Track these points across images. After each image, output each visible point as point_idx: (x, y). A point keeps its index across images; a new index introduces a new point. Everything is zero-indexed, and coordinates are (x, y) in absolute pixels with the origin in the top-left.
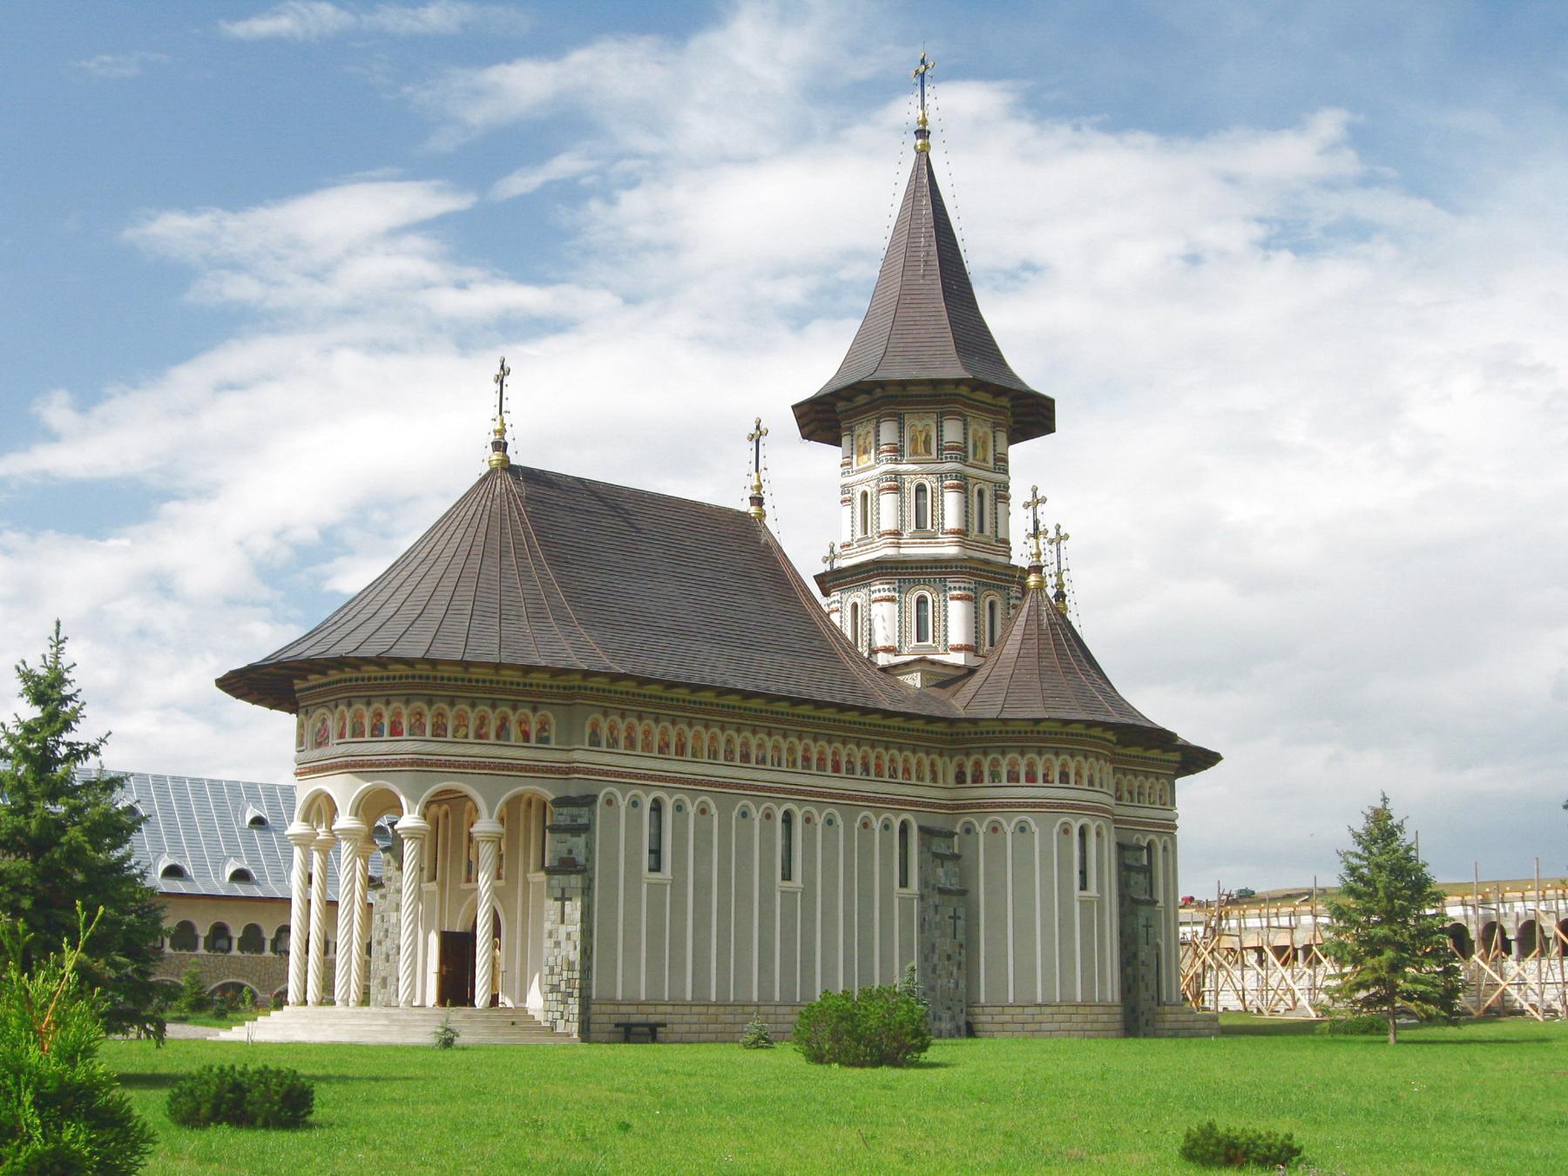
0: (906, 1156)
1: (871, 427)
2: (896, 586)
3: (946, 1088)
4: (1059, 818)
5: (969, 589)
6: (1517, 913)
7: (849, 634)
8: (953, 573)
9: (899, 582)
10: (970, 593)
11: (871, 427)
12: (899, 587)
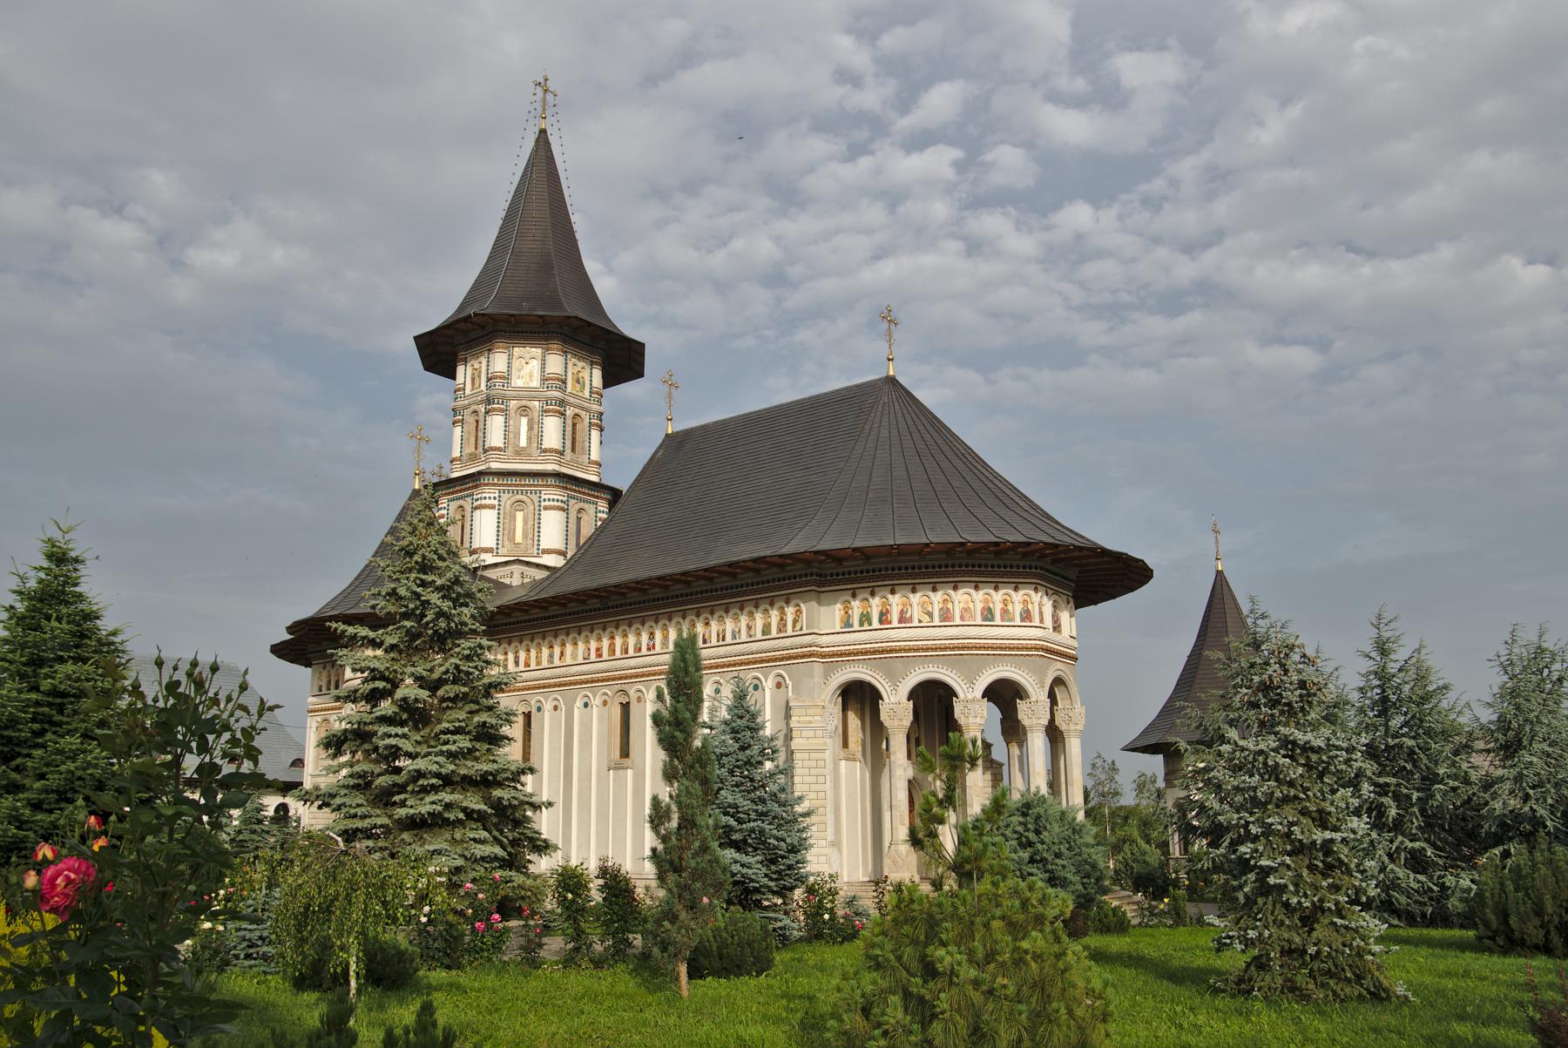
2: (497, 495)
10: (563, 505)
11: (537, 351)
12: (500, 496)
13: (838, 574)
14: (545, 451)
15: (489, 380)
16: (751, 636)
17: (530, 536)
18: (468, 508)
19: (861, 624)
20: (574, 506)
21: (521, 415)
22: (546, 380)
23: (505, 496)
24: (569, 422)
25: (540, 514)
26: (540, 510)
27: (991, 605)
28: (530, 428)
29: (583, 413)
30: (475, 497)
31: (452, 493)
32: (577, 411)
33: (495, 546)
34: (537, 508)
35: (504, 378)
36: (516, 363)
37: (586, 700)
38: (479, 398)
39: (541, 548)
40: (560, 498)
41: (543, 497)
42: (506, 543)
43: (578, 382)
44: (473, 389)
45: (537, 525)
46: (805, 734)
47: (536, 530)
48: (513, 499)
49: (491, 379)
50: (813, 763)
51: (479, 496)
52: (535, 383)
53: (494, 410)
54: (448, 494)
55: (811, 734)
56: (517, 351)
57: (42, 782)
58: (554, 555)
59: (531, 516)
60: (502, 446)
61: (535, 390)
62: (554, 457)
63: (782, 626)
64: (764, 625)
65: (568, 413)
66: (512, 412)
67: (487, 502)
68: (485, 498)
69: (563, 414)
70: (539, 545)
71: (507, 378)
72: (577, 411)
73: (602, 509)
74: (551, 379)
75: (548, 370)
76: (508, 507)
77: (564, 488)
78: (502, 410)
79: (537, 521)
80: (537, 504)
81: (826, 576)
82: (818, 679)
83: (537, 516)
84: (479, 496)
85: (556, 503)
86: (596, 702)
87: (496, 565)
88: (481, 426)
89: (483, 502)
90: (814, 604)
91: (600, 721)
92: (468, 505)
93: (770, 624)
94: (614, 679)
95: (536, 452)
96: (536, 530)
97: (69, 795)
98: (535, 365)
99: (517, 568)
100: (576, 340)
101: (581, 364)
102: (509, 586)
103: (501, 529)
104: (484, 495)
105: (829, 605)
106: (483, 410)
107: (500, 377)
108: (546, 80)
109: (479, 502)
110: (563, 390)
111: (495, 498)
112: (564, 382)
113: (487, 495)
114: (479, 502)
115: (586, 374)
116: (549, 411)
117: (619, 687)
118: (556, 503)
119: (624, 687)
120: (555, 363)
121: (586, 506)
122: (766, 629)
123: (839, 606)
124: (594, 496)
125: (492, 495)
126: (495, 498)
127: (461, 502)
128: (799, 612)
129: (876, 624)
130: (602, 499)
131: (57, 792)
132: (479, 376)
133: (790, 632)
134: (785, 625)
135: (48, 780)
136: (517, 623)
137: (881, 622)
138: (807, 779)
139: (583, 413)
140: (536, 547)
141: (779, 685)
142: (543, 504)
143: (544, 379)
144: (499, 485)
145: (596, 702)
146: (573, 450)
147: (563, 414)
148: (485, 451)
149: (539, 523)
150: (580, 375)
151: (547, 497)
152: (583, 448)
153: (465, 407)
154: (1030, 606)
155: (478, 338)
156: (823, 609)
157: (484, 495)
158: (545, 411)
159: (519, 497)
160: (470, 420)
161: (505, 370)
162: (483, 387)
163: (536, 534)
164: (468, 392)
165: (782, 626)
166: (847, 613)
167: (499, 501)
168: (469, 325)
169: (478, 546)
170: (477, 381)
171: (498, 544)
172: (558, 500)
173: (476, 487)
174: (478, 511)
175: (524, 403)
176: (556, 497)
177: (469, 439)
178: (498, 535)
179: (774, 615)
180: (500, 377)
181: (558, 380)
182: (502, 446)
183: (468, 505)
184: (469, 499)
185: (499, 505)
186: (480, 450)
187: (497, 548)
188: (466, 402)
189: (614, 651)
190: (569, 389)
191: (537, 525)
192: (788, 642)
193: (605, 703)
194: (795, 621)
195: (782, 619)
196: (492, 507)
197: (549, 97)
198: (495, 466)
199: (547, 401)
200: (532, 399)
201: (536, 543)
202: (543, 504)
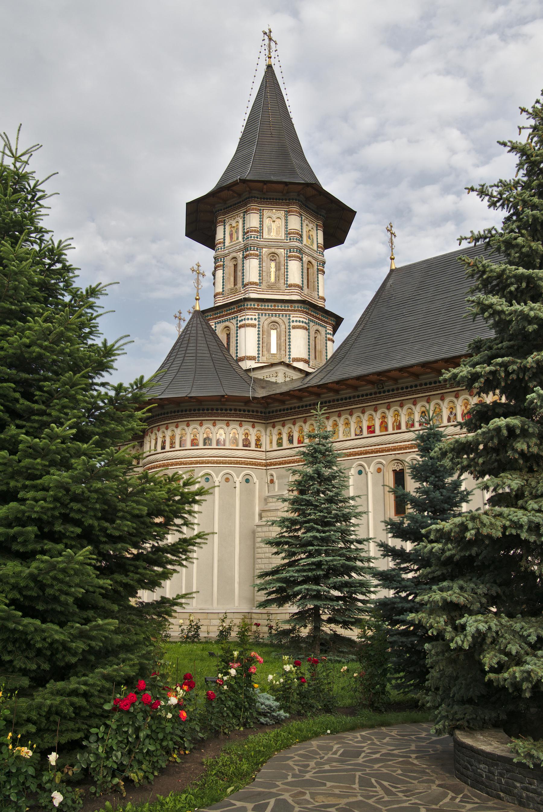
0: (217, 733)
1: (282, 214)
2: (257, 317)
3: (494, 641)
4: (243, 471)
5: (305, 323)
6: (494, 501)
7: (225, 342)
8: (295, 311)
9: (259, 315)
10: (306, 325)
11: (282, 214)
12: (259, 318)
14: (290, 286)
15: (245, 233)
17: (283, 348)
18: (233, 328)
20: (313, 327)
21: (271, 260)
22: (289, 234)
23: (263, 318)
24: (305, 266)
25: (290, 332)
26: (289, 329)
28: (278, 269)
30: (239, 319)
31: (219, 317)
32: (310, 259)
33: (257, 356)
34: (287, 327)
35: (257, 232)
36: (267, 222)
37: (360, 468)
38: (238, 248)
39: (291, 357)
40: (304, 320)
41: (292, 319)
42: (265, 353)
43: (309, 238)
44: (231, 241)
45: (288, 340)
47: (288, 344)
48: (269, 320)
49: (248, 232)
51: (243, 318)
52: (282, 236)
53: (251, 255)
54: (216, 318)
56: (266, 213)
57: (13, 504)
58: (302, 363)
59: (283, 333)
61: (280, 241)
62: (297, 290)
65: (304, 259)
66: (265, 257)
67: (250, 322)
68: (248, 319)
69: (301, 259)
70: (290, 355)
71: (260, 231)
73: (330, 332)
74: (293, 233)
76: (266, 326)
77: (307, 313)
78: (256, 255)
79: (288, 337)
80: (287, 324)
83: (287, 334)
84: (243, 318)
85: (301, 324)
86: (371, 469)
87: (254, 369)
88: (240, 268)
89: (247, 322)
91: (375, 484)
92: (232, 325)
94: (389, 450)
95: (283, 287)
96: (288, 344)
97: (58, 528)
98: (281, 223)
99: (281, 369)
100: (307, 207)
101: (311, 225)
102: (276, 383)
103: (261, 342)
104: (247, 317)
106: (241, 256)
107: (255, 231)
109: (243, 322)
110: (301, 241)
111: (255, 319)
112: (301, 236)
113: (250, 317)
114: (243, 322)
115: (313, 233)
116: (293, 256)
117: (393, 457)
118: (301, 324)
119: (398, 457)
120: (295, 222)
121: (320, 328)
124: (325, 322)
125: (254, 317)
126: (255, 319)
127: (227, 324)
130: (330, 324)
131: (38, 522)
132: (237, 232)
135: (23, 501)
136: (291, 409)
140: (288, 357)
142: (292, 324)
143: (287, 234)
144: (258, 309)
145: (371, 469)
146: (308, 287)
147: (301, 259)
148: (244, 286)
149: (289, 339)
150: (311, 233)
151: (295, 319)
152: (314, 287)
153: (225, 256)
155: (235, 204)
157: (247, 317)
158: (289, 257)
159: (273, 319)
160: (230, 264)
161: (258, 226)
162: (240, 239)
163: (288, 347)
164: (227, 244)
167: (259, 321)
168: (231, 192)
169: (244, 355)
170: (235, 236)
171: (259, 354)
172: (303, 322)
173: (240, 311)
174: (242, 330)
175: (273, 250)
176: (301, 319)
177: (229, 278)
178: (259, 347)
180: (255, 231)
182: (258, 281)
183: (232, 325)
184: (234, 321)
185: (259, 324)
186: (239, 285)
187: (259, 357)
188: (227, 252)
190: (305, 242)
191: (288, 340)
193: (379, 470)
196: (253, 326)
197: (273, 44)
198: (253, 296)
199: (290, 249)
200: (279, 247)
201: (288, 353)
202: (292, 324)
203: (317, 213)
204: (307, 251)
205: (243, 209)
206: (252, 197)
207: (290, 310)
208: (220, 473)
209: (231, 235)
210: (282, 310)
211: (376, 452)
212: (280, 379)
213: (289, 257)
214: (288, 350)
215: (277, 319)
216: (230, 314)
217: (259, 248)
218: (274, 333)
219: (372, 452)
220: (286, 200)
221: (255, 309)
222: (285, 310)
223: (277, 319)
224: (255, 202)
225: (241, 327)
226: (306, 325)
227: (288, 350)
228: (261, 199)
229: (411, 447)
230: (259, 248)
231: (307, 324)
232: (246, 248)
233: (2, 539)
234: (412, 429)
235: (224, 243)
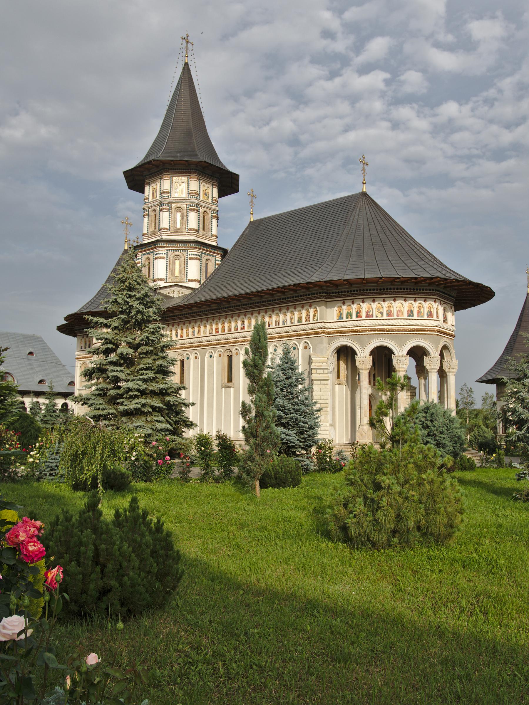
2: (166, 252)
5: (198, 255)
8: (191, 248)
10: (198, 257)
11: (185, 179)
13: (336, 293)
14: (190, 230)
15: (161, 194)
16: (292, 323)
17: (183, 273)
19: (347, 318)
20: (204, 258)
22: (190, 194)
23: (170, 253)
24: (201, 215)
27: (412, 309)
29: (208, 211)
30: (155, 253)
31: (144, 251)
33: (165, 278)
34: (186, 259)
35: (169, 193)
37: (211, 354)
38: (156, 203)
40: (197, 254)
41: (189, 253)
43: (206, 194)
44: (153, 198)
45: (186, 267)
46: (318, 371)
48: (174, 254)
50: (322, 386)
52: (184, 195)
53: (164, 209)
54: (142, 252)
55: (321, 371)
56: (175, 179)
58: (194, 282)
60: (168, 227)
62: (194, 233)
63: (308, 318)
64: (299, 318)
65: (201, 210)
66: (173, 210)
69: (198, 211)
71: (170, 193)
72: (205, 209)
74: (192, 193)
75: (190, 189)
76: (171, 258)
78: (168, 209)
81: (330, 293)
82: (325, 344)
85: (195, 256)
86: (216, 355)
89: (159, 256)
90: (323, 307)
92: (151, 257)
93: (301, 317)
94: (225, 344)
95: (185, 231)
96: (186, 269)
98: (184, 186)
99: (176, 289)
100: (204, 173)
101: (207, 185)
102: (173, 298)
103: (168, 269)
104: (159, 252)
105: (331, 308)
106: (158, 209)
107: (167, 192)
108: (188, 36)
109: (157, 256)
110: (198, 199)
111: (165, 254)
112: (199, 195)
113: (161, 252)
114: (157, 256)
117: (227, 348)
120: (194, 185)
121: (210, 258)
122: (300, 320)
123: (336, 308)
124: (214, 253)
125: (164, 252)
126: (165, 254)
127: (148, 256)
128: (316, 311)
129: (354, 318)
130: (218, 254)
132: (156, 192)
133: (311, 321)
134: (309, 318)
137: (357, 317)
138: (319, 394)
139: (208, 211)
140: (185, 278)
141: (306, 348)
142: (189, 256)
143: (189, 193)
144: (167, 247)
145: (216, 355)
146: (204, 229)
147: (198, 211)
148: (160, 230)
151: (191, 253)
153: (149, 208)
154: (432, 310)
156: (328, 310)
157: (159, 252)
158: (189, 210)
159: (177, 253)
160: (152, 214)
161: (169, 188)
162: (158, 198)
163: (186, 272)
164: (151, 200)
165: (308, 318)
166: (340, 312)
172: (196, 255)
173: (156, 248)
174: (156, 260)
175: (179, 205)
179: (304, 312)
180: (167, 192)
181: (196, 193)
182: (168, 227)
184: (152, 254)
186: (157, 229)
188: (150, 205)
189: (224, 330)
191: (186, 267)
192: (310, 326)
193: (220, 355)
194: (314, 316)
195: (307, 315)
196: (164, 258)
197: (190, 45)
198: (165, 237)
199: (190, 204)
200: (183, 203)
201: (185, 276)
202: (189, 256)
203: (213, 176)
204: (203, 204)
205: (160, 176)
206: (165, 169)
207: (188, 247)
208: (405, 342)
209: (153, 194)
210: (182, 247)
211: (219, 345)
212: (176, 295)
213: (189, 210)
214: (185, 274)
215: (179, 253)
216: (150, 249)
217: (169, 204)
218: (177, 262)
219: (217, 345)
220: (188, 170)
221: (164, 247)
222: (185, 247)
223: (179, 253)
224: (167, 172)
225: (156, 259)
226: (198, 257)
227: (185, 274)
228: (171, 169)
229: (247, 341)
230: (169, 204)
231: (200, 256)
232: (161, 204)
233: (3, 639)
234: (243, 331)
235: (149, 199)
